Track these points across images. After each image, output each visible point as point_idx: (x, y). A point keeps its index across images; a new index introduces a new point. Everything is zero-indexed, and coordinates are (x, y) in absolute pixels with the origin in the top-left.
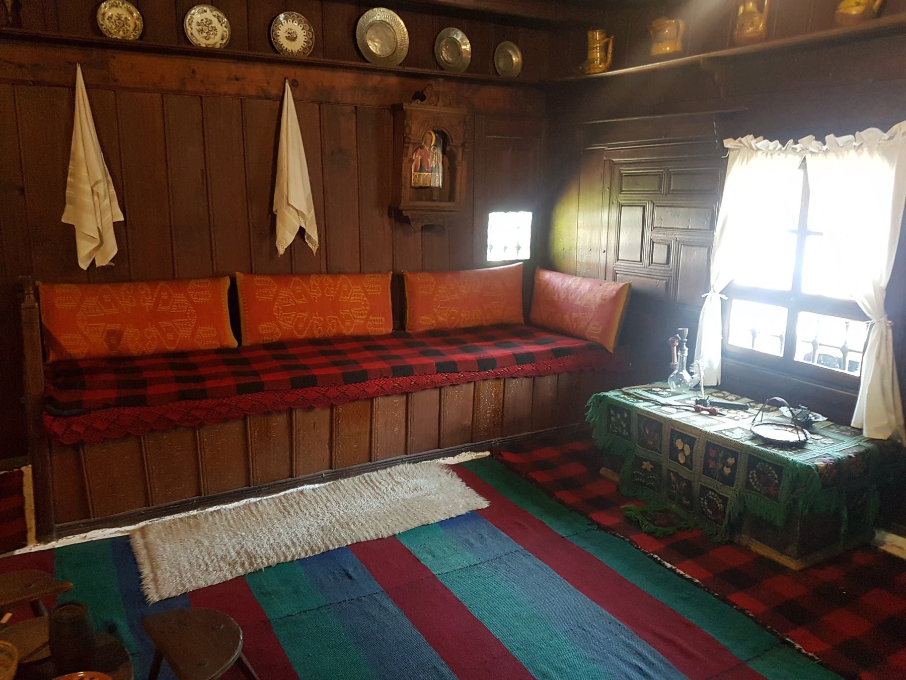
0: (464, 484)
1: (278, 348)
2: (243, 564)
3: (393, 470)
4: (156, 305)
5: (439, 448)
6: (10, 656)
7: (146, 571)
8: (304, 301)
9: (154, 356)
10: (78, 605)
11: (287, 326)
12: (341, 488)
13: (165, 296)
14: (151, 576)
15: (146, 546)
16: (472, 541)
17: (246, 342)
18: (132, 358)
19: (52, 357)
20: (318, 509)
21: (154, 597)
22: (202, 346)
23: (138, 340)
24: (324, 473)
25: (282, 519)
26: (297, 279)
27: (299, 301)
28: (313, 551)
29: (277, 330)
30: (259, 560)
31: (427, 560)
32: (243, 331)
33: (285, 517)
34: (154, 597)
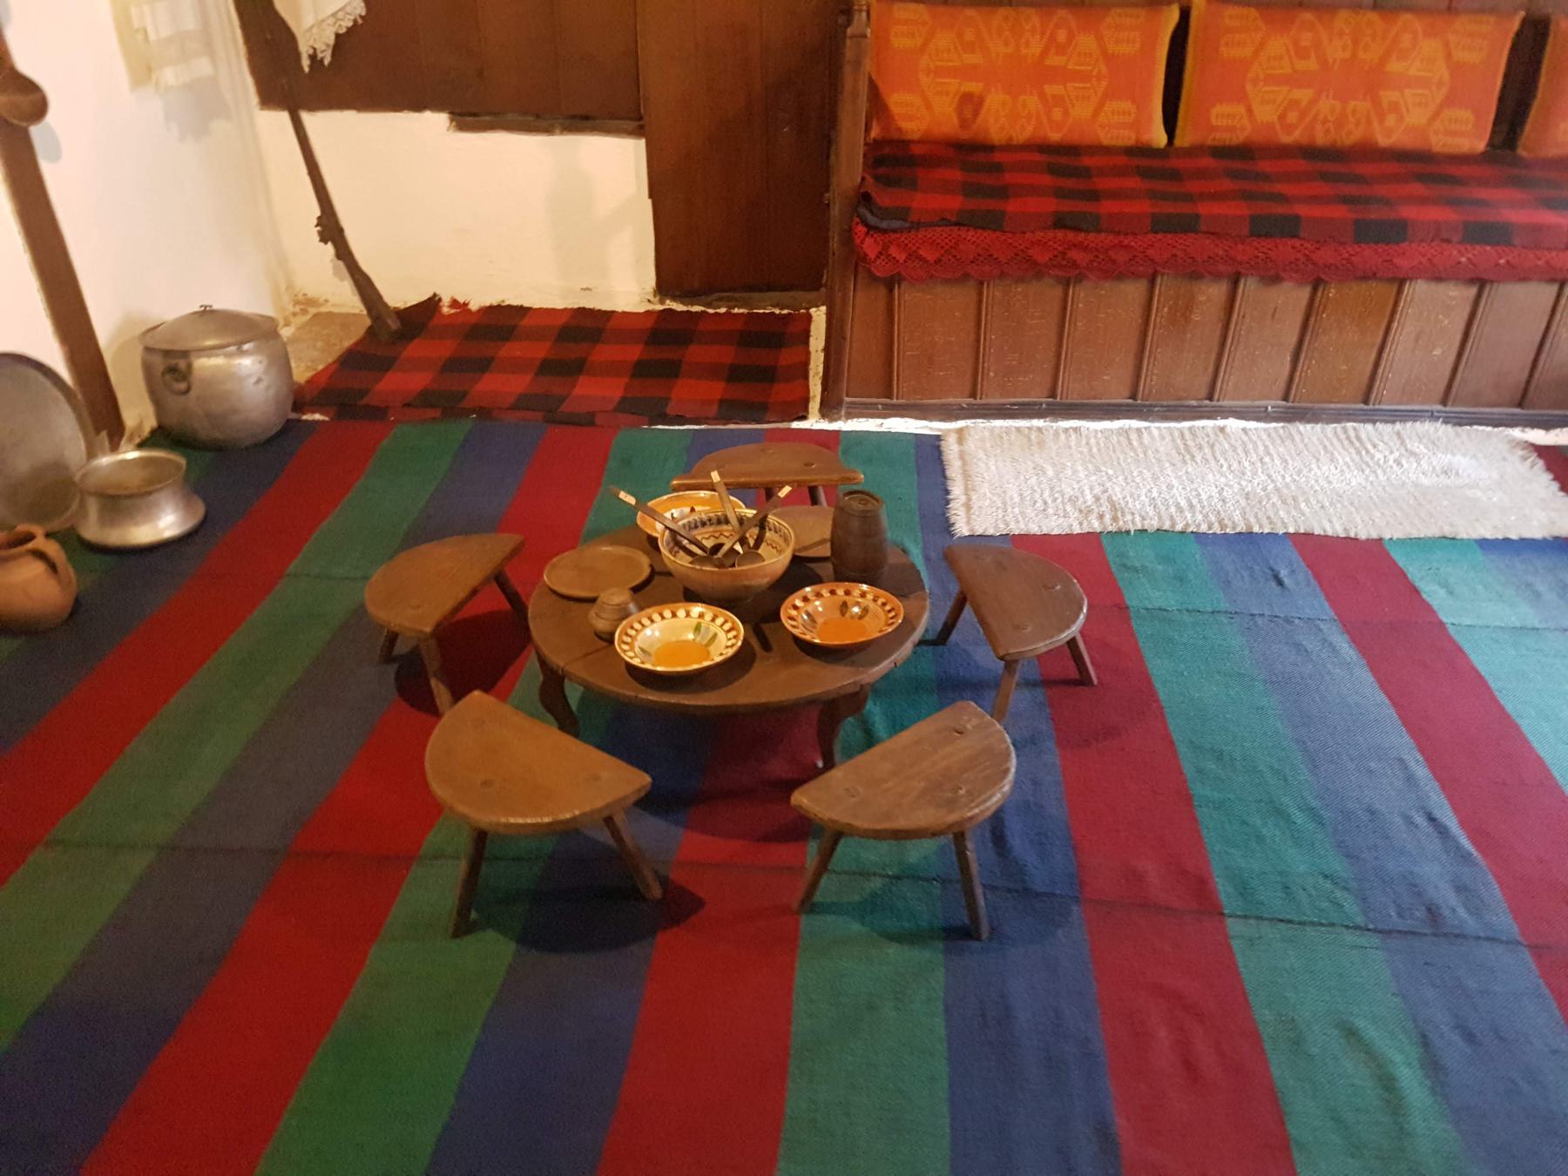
0: (1555, 486)
1: (1241, 154)
2: (1101, 517)
3: (1407, 428)
4: (1045, 53)
5: (1520, 405)
6: (786, 540)
7: (957, 490)
8: (1312, 64)
9: (1028, 147)
10: (871, 496)
11: (1266, 114)
12: (1297, 438)
13: (1062, 36)
14: (963, 499)
15: (962, 456)
16: (1541, 588)
17: (1183, 139)
18: (990, 148)
19: (875, 133)
20: (1247, 464)
21: (962, 528)
22: (1106, 138)
23: (1008, 118)
24: (1271, 404)
25: (1179, 465)
26: (1308, 16)
27: (1301, 65)
28: (1223, 526)
29: (1245, 121)
30: (1129, 517)
31: (1433, 594)
32: (1180, 123)
33: (1184, 462)
34: (962, 528)
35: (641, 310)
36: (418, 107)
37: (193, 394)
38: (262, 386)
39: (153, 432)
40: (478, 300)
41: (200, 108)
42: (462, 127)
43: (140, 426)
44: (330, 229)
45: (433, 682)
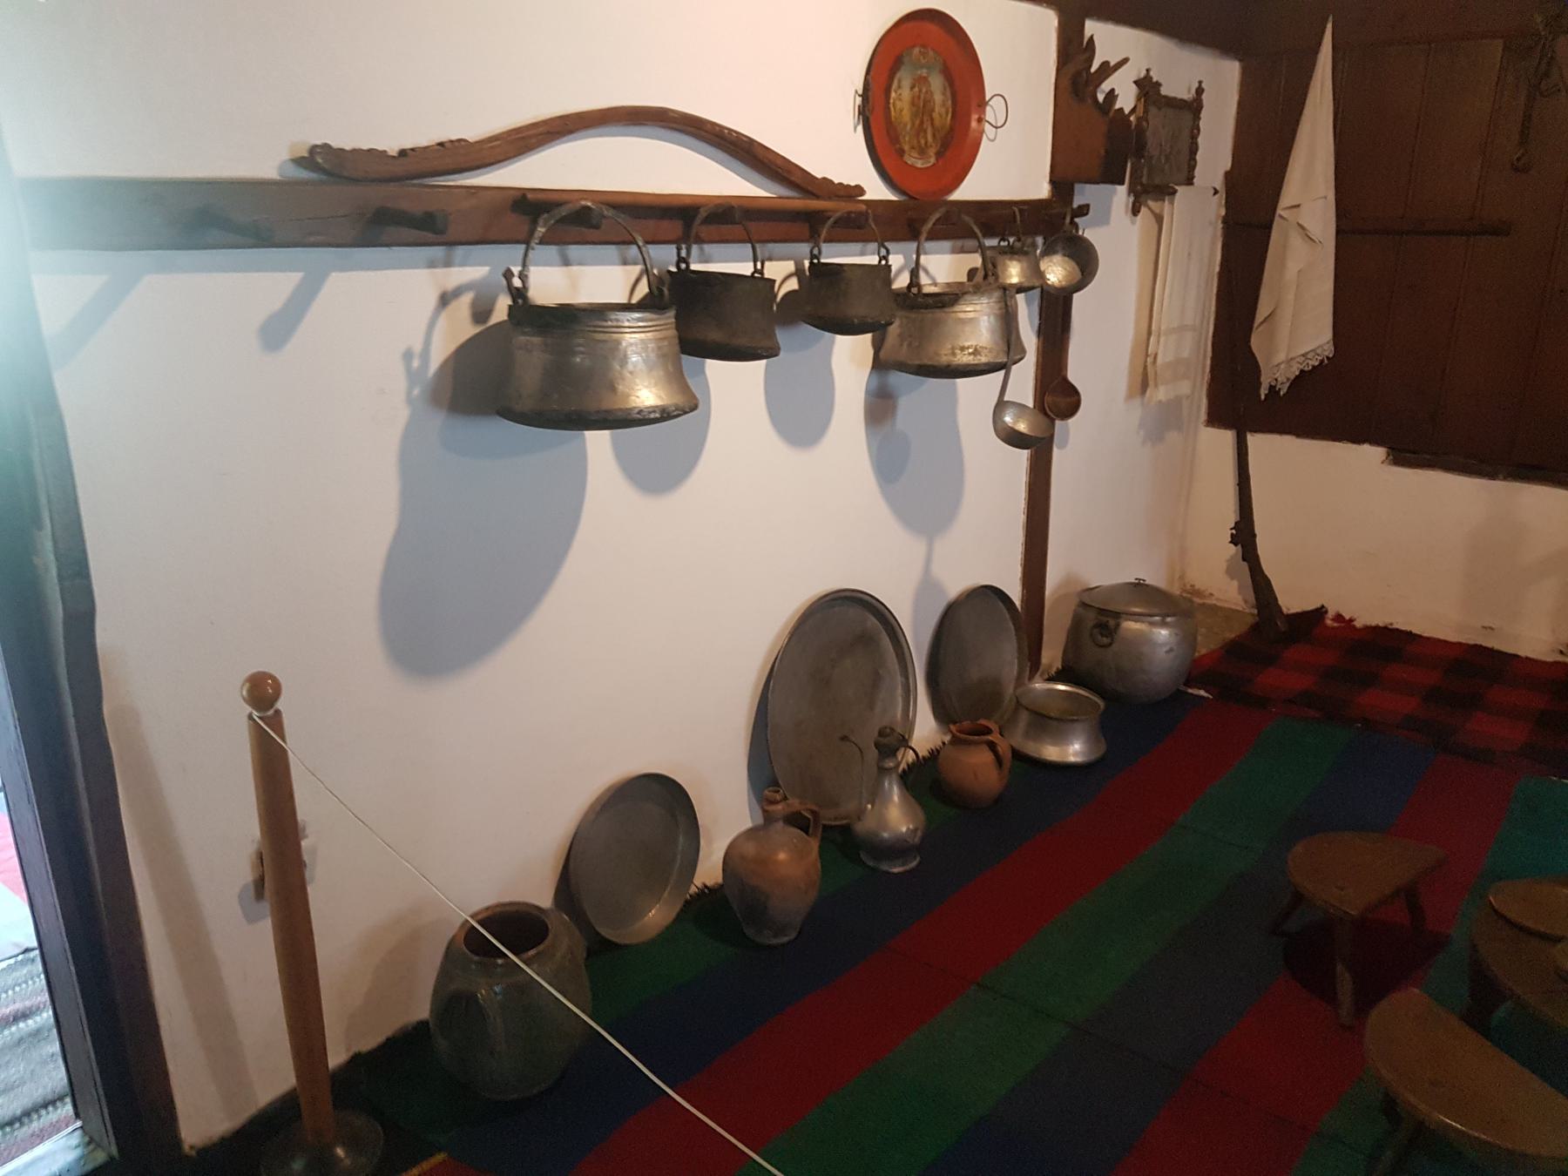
35: (1550, 659)
36: (1357, 439)
37: (1115, 647)
38: (1172, 655)
39: (1058, 672)
40: (1366, 616)
41: (1164, 422)
42: (1398, 461)
43: (1050, 666)
44: (1244, 535)
45: (1339, 968)
